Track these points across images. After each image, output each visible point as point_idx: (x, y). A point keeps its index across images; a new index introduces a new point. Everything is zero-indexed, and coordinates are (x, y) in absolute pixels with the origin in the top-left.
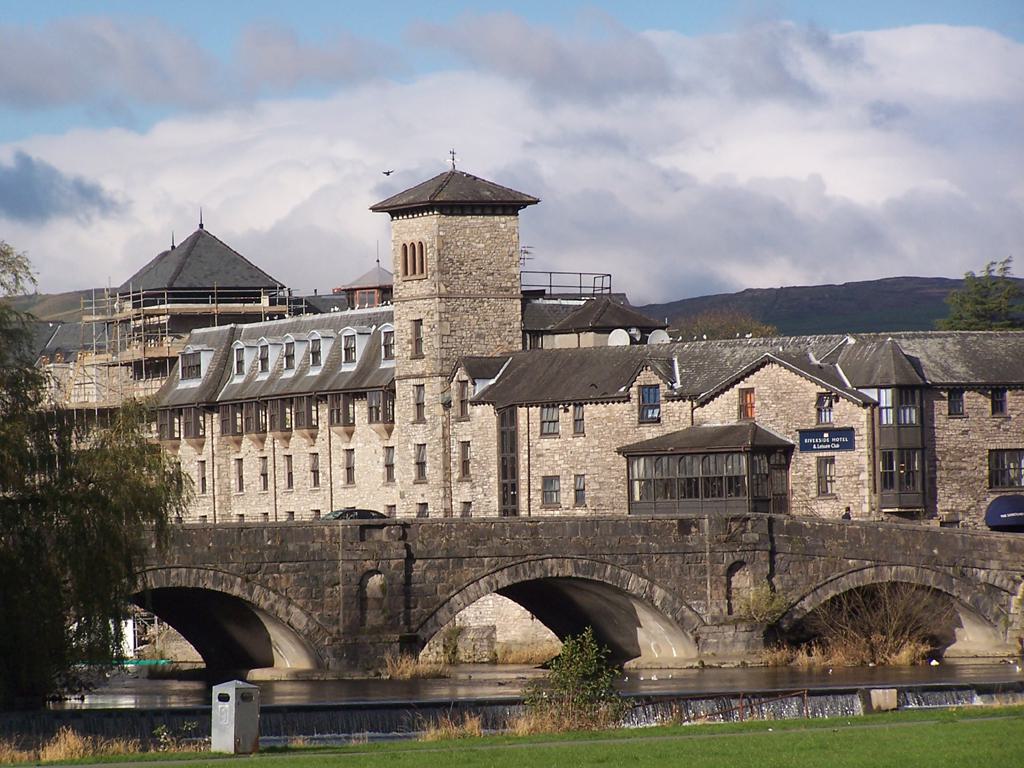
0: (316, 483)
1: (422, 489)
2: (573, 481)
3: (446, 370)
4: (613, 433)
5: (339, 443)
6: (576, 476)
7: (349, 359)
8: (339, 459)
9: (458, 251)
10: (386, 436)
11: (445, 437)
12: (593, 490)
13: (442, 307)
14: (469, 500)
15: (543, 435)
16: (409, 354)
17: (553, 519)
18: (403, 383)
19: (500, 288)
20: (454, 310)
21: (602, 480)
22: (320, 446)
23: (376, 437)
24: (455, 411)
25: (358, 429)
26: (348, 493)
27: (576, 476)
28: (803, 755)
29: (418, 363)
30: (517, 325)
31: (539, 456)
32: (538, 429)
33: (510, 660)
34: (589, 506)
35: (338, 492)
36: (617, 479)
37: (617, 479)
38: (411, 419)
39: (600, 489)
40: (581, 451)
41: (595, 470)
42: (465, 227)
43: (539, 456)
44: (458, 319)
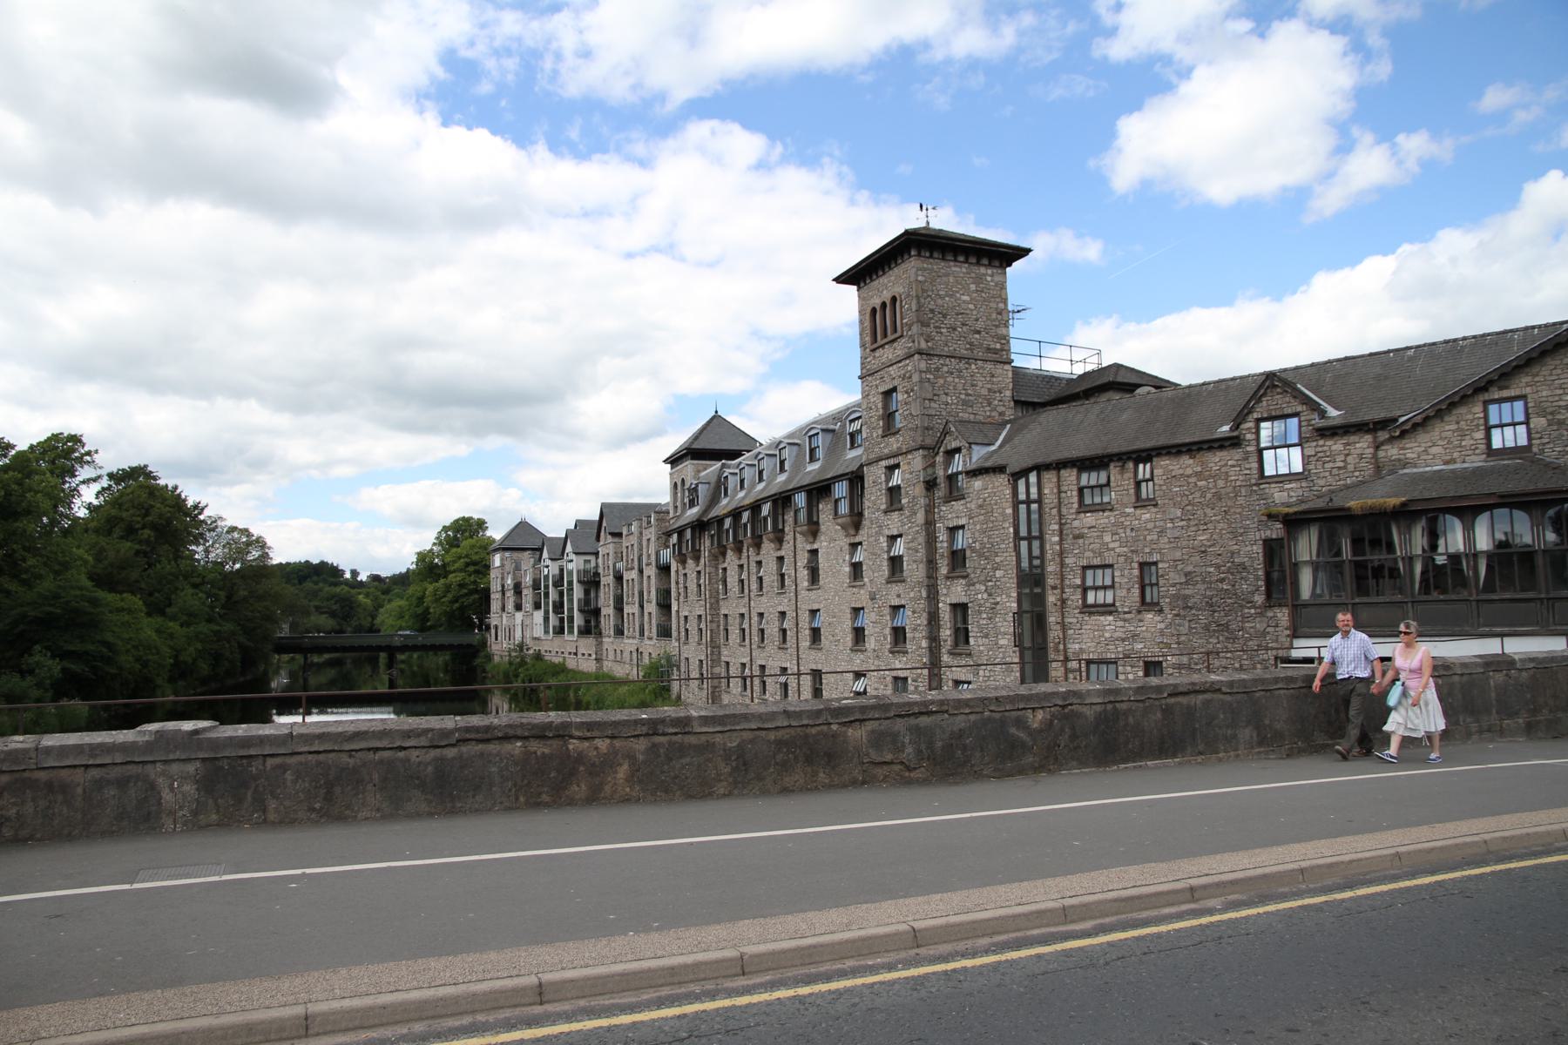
0: (783, 585)
1: (896, 588)
2: (1136, 572)
3: (929, 441)
4: (1209, 496)
5: (804, 546)
6: (1142, 565)
7: (812, 459)
8: (803, 559)
9: (940, 302)
10: (852, 532)
11: (930, 524)
12: (1174, 585)
13: (923, 365)
14: (964, 600)
15: (1083, 508)
16: (880, 432)
17: (1452, 471)
18: (873, 468)
19: (989, 349)
20: (937, 369)
21: (1190, 568)
22: (786, 551)
23: (841, 533)
24: (941, 491)
25: (823, 528)
26: (813, 595)
27: (1142, 565)
28: (134, 575)
29: (892, 440)
30: (1008, 393)
31: (1077, 537)
32: (1075, 499)
33: (198, 764)
34: (1166, 610)
35: (803, 594)
36: (1218, 567)
37: (1218, 567)
38: (883, 507)
39: (1187, 583)
40: (1150, 525)
41: (1178, 555)
42: (947, 275)
43: (1077, 537)
44: (941, 381)
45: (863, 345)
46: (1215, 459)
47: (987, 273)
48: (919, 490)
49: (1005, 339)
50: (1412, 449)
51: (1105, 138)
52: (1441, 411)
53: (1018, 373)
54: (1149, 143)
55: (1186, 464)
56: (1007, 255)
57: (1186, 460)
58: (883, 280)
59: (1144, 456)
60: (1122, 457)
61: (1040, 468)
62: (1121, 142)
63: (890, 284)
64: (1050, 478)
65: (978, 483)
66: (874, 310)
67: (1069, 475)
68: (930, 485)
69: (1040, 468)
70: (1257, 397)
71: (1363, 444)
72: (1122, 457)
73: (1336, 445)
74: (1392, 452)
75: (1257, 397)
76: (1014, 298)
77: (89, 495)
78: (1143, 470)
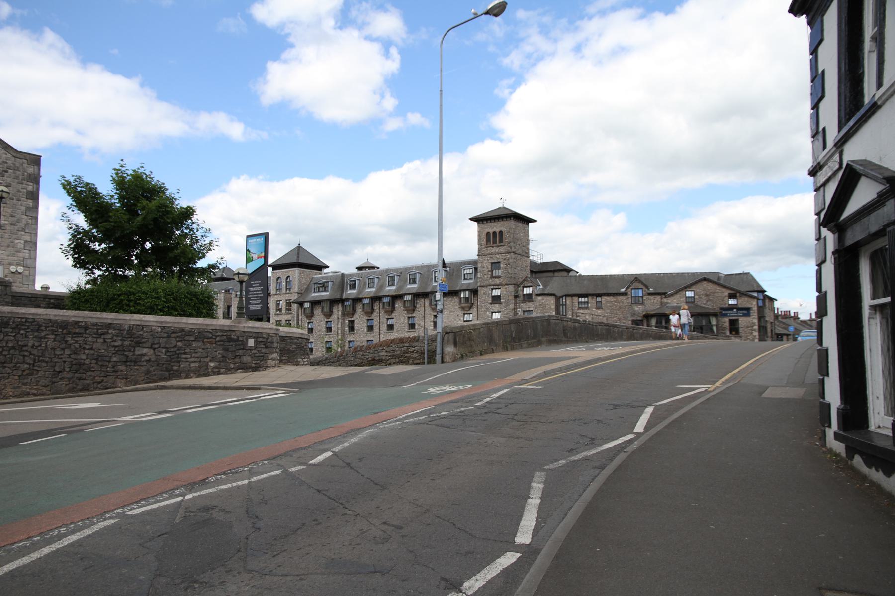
45: (480, 244)
46: (620, 298)
47: (520, 225)
48: (511, 298)
49: (528, 249)
50: (669, 300)
51: (260, 71)
52: (676, 292)
53: (533, 264)
54: (284, 81)
55: (611, 299)
56: (527, 221)
57: (611, 297)
58: (495, 224)
59: (600, 295)
60: (592, 295)
61: (566, 295)
62: (269, 77)
63: (496, 227)
64: (569, 299)
65: (540, 298)
66: (488, 234)
67: (575, 298)
68: (516, 297)
69: (566, 295)
70: (632, 282)
71: (658, 298)
72: (592, 295)
73: (652, 297)
74: (665, 300)
75: (632, 282)
76: (532, 235)
77: (98, 273)
78: (599, 299)
